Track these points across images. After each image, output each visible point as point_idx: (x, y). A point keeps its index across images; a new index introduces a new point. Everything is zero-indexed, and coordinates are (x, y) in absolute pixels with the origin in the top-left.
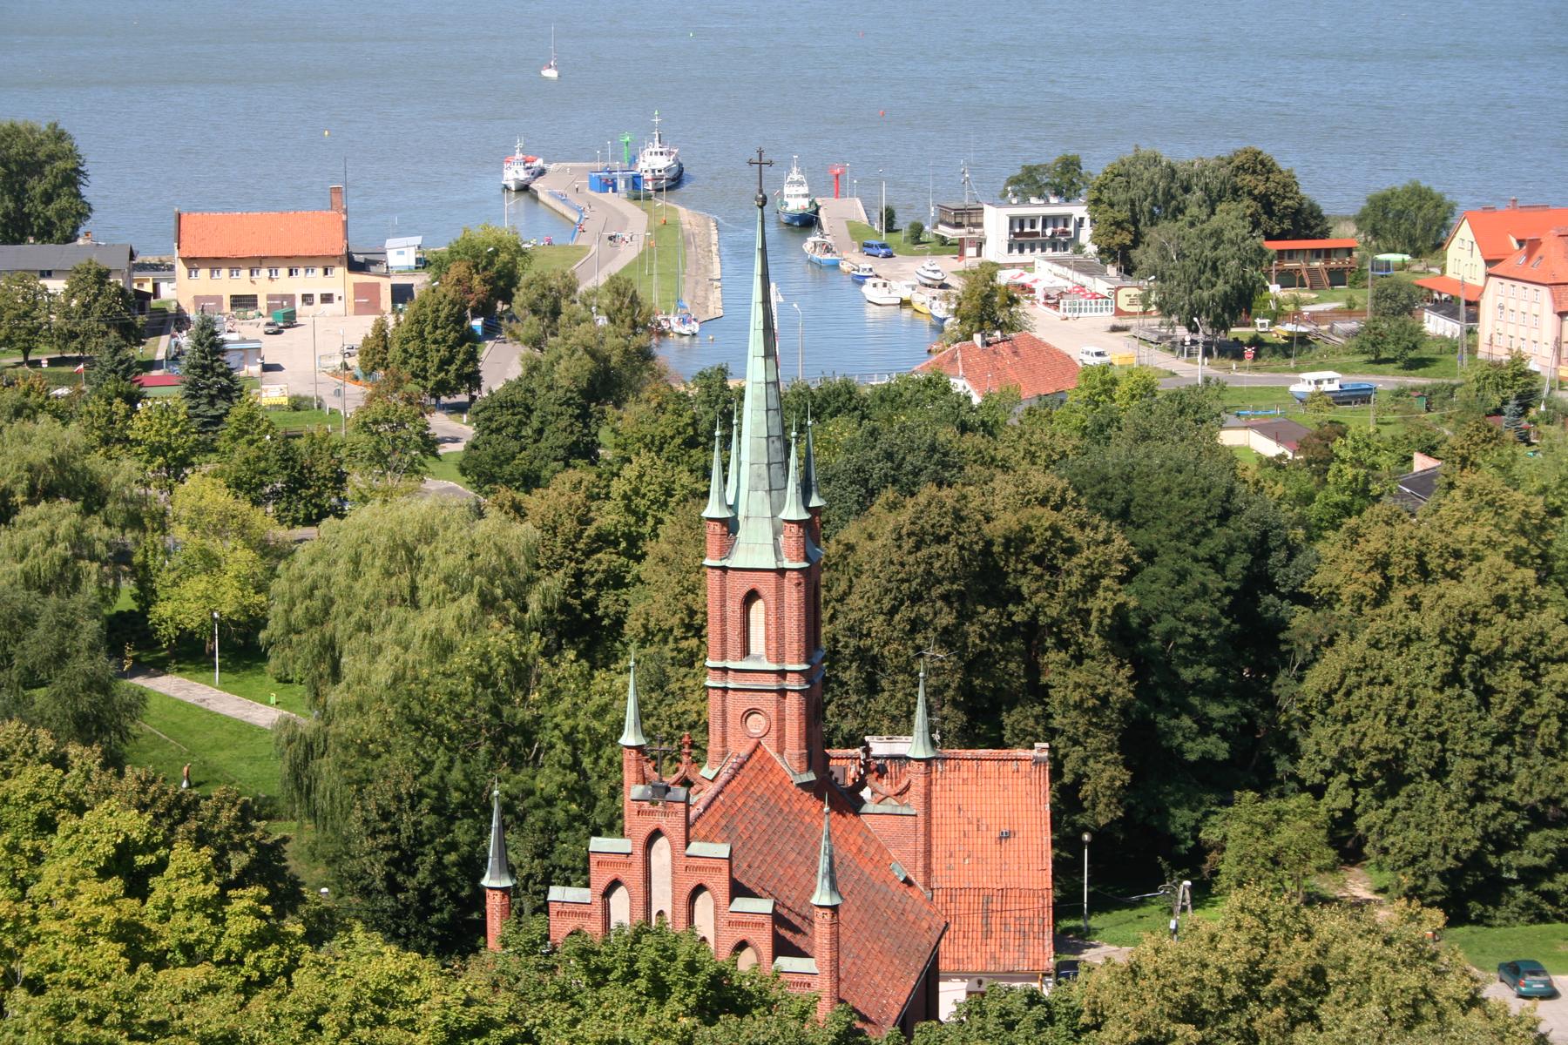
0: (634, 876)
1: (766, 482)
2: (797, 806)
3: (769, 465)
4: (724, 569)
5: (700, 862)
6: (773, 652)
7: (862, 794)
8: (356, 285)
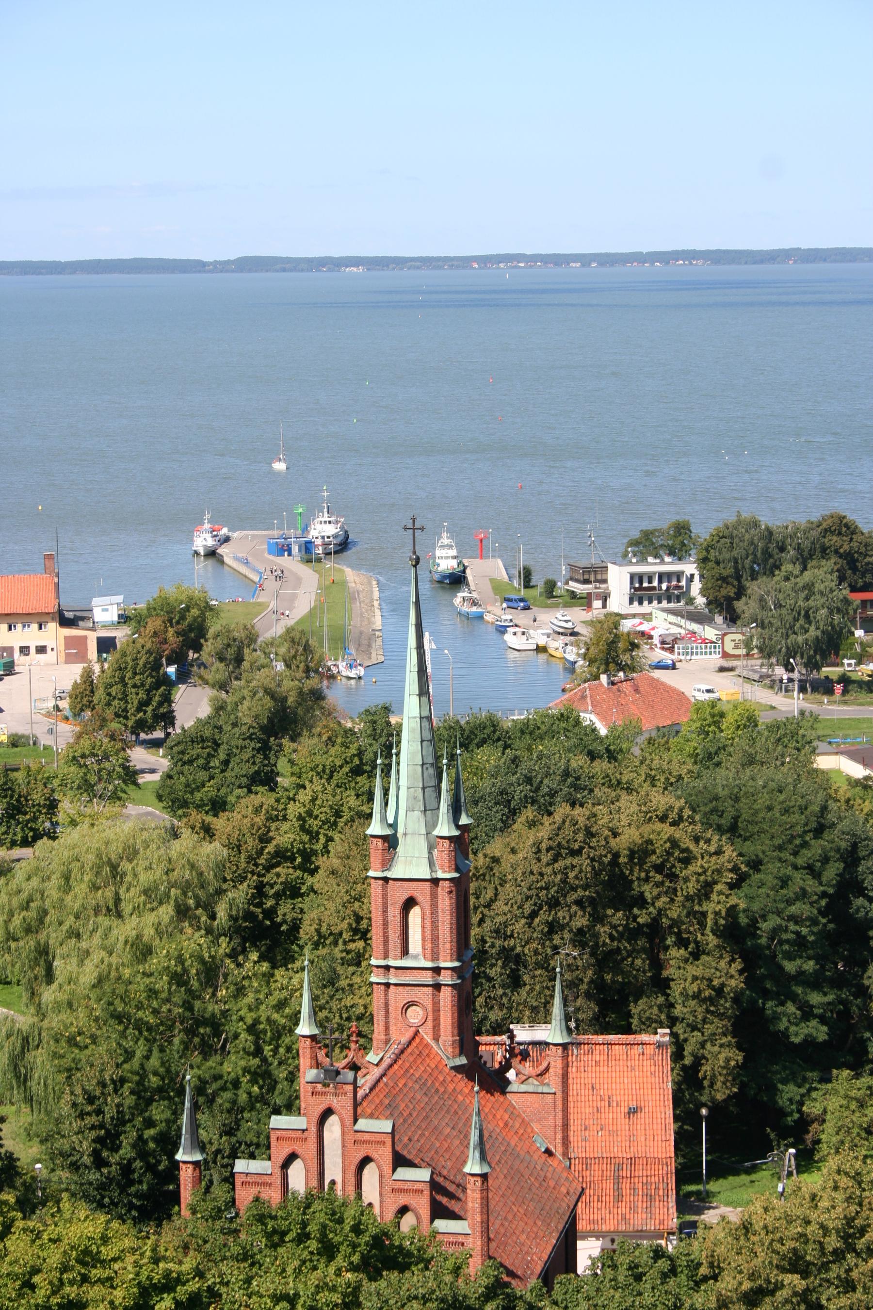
0: (309, 1149)
1: (421, 804)
2: (451, 1087)
3: (424, 788)
4: (386, 880)
5: (366, 1137)
6: (428, 951)
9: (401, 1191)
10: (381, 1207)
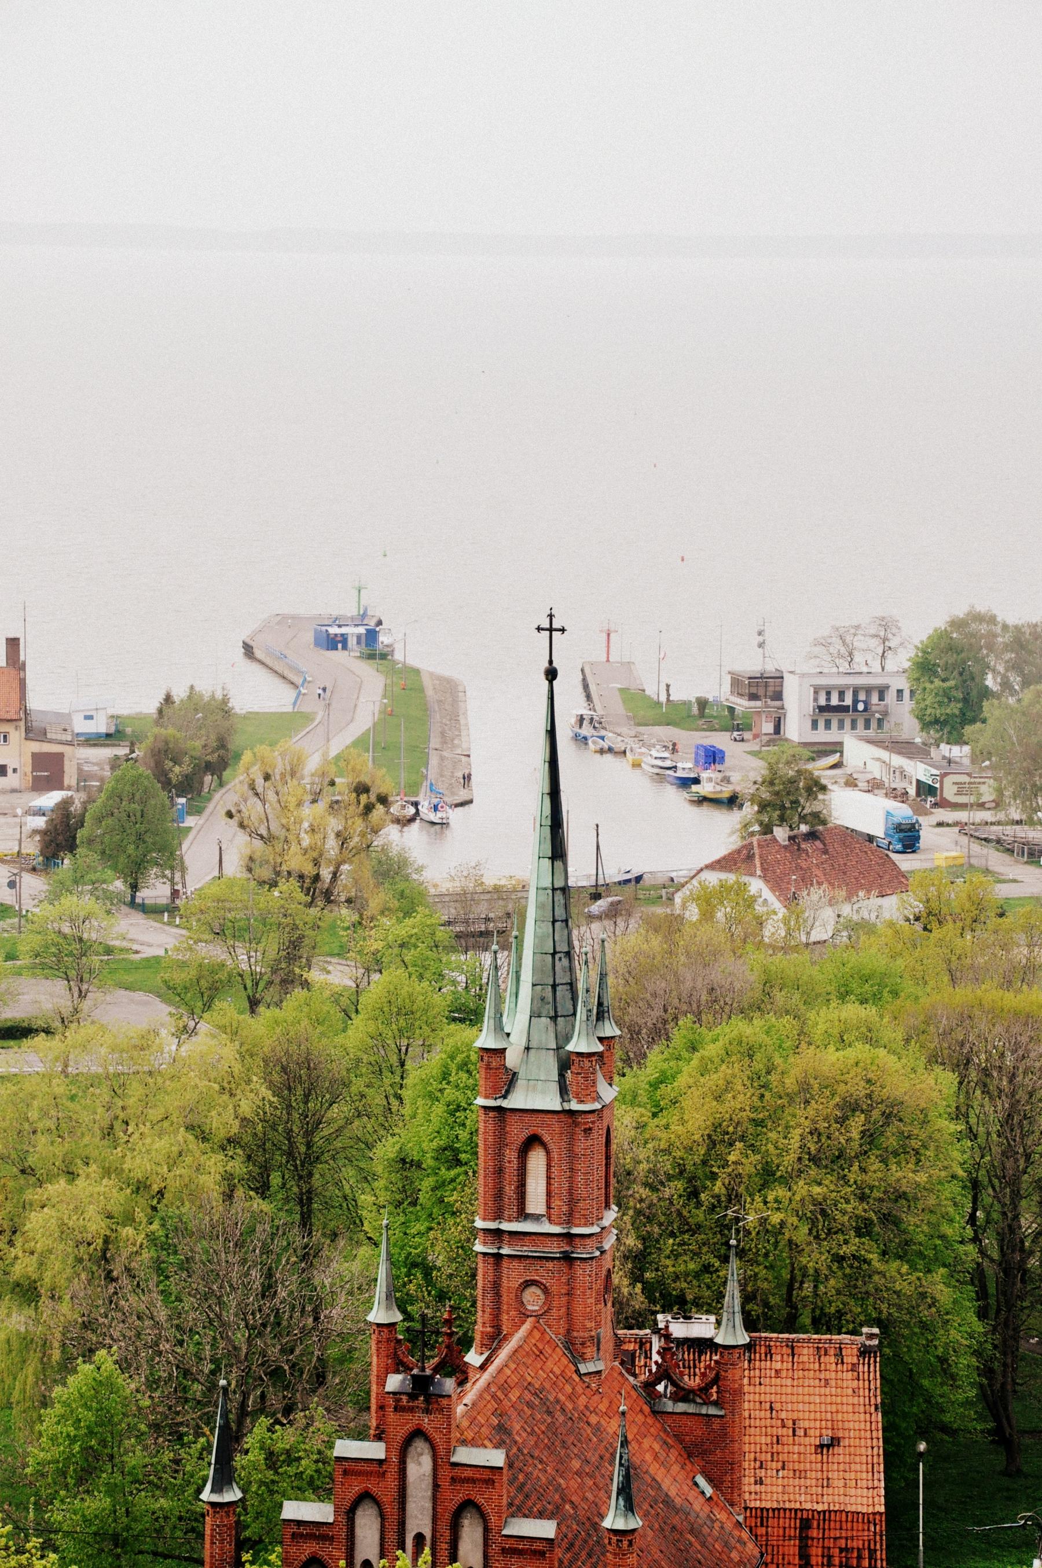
5: (468, 1473)
7: (466, 1359)
8: (35, 756)
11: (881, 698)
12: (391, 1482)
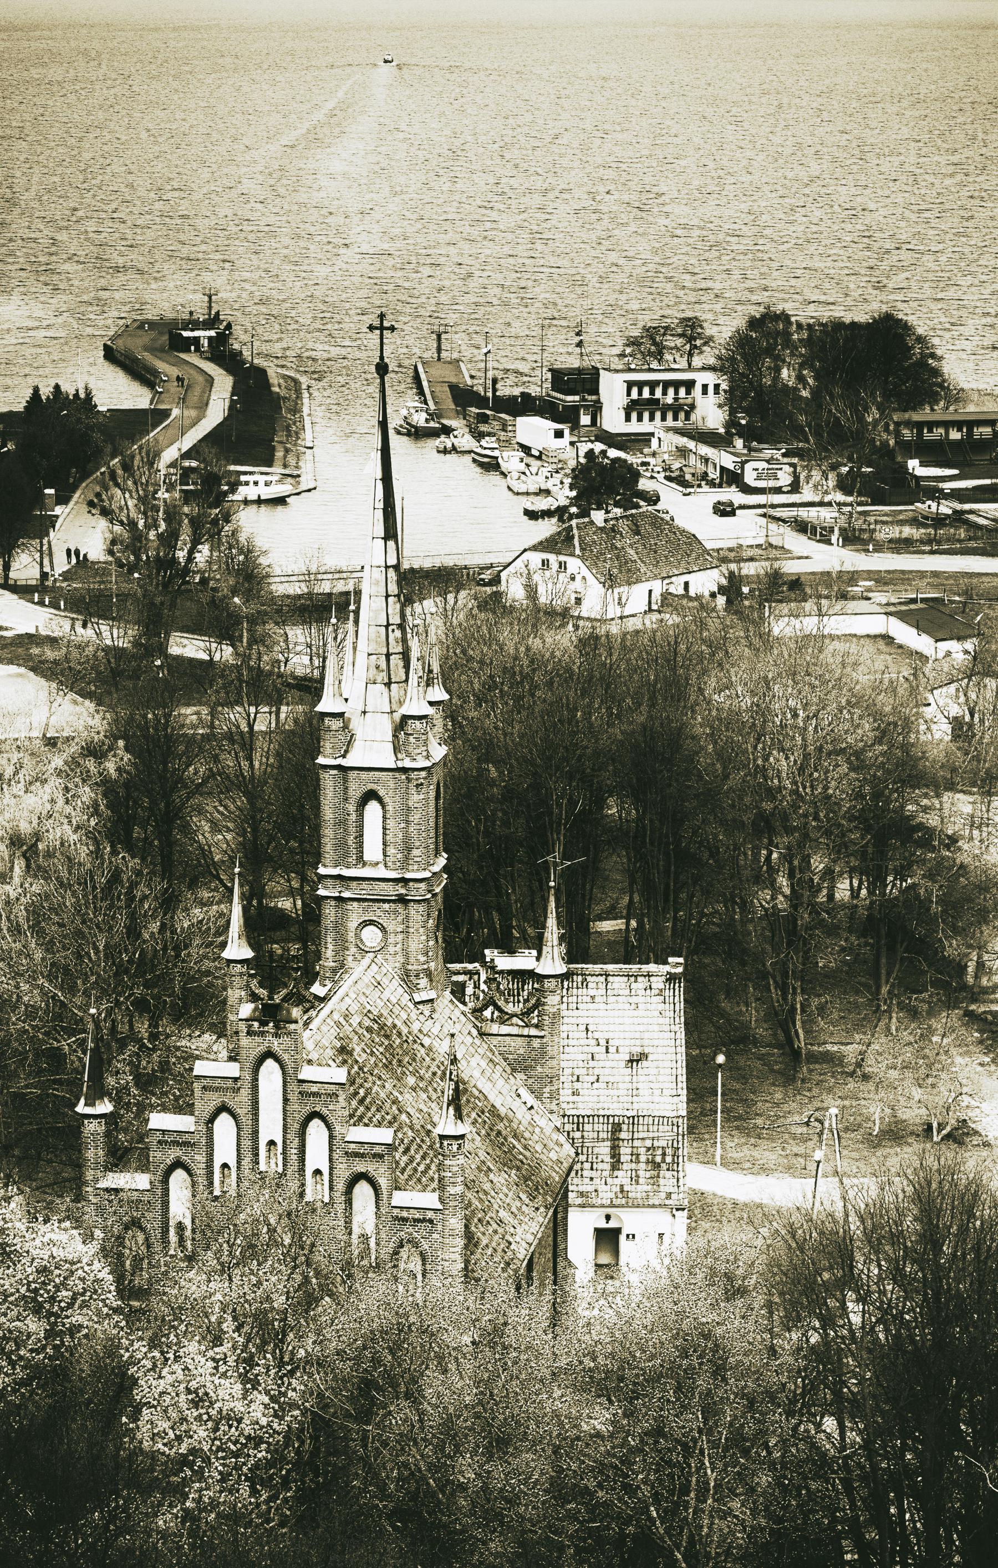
5: (314, 1088)
9: (356, 1155)
10: (331, 1174)
11: (688, 393)
12: (245, 1094)
